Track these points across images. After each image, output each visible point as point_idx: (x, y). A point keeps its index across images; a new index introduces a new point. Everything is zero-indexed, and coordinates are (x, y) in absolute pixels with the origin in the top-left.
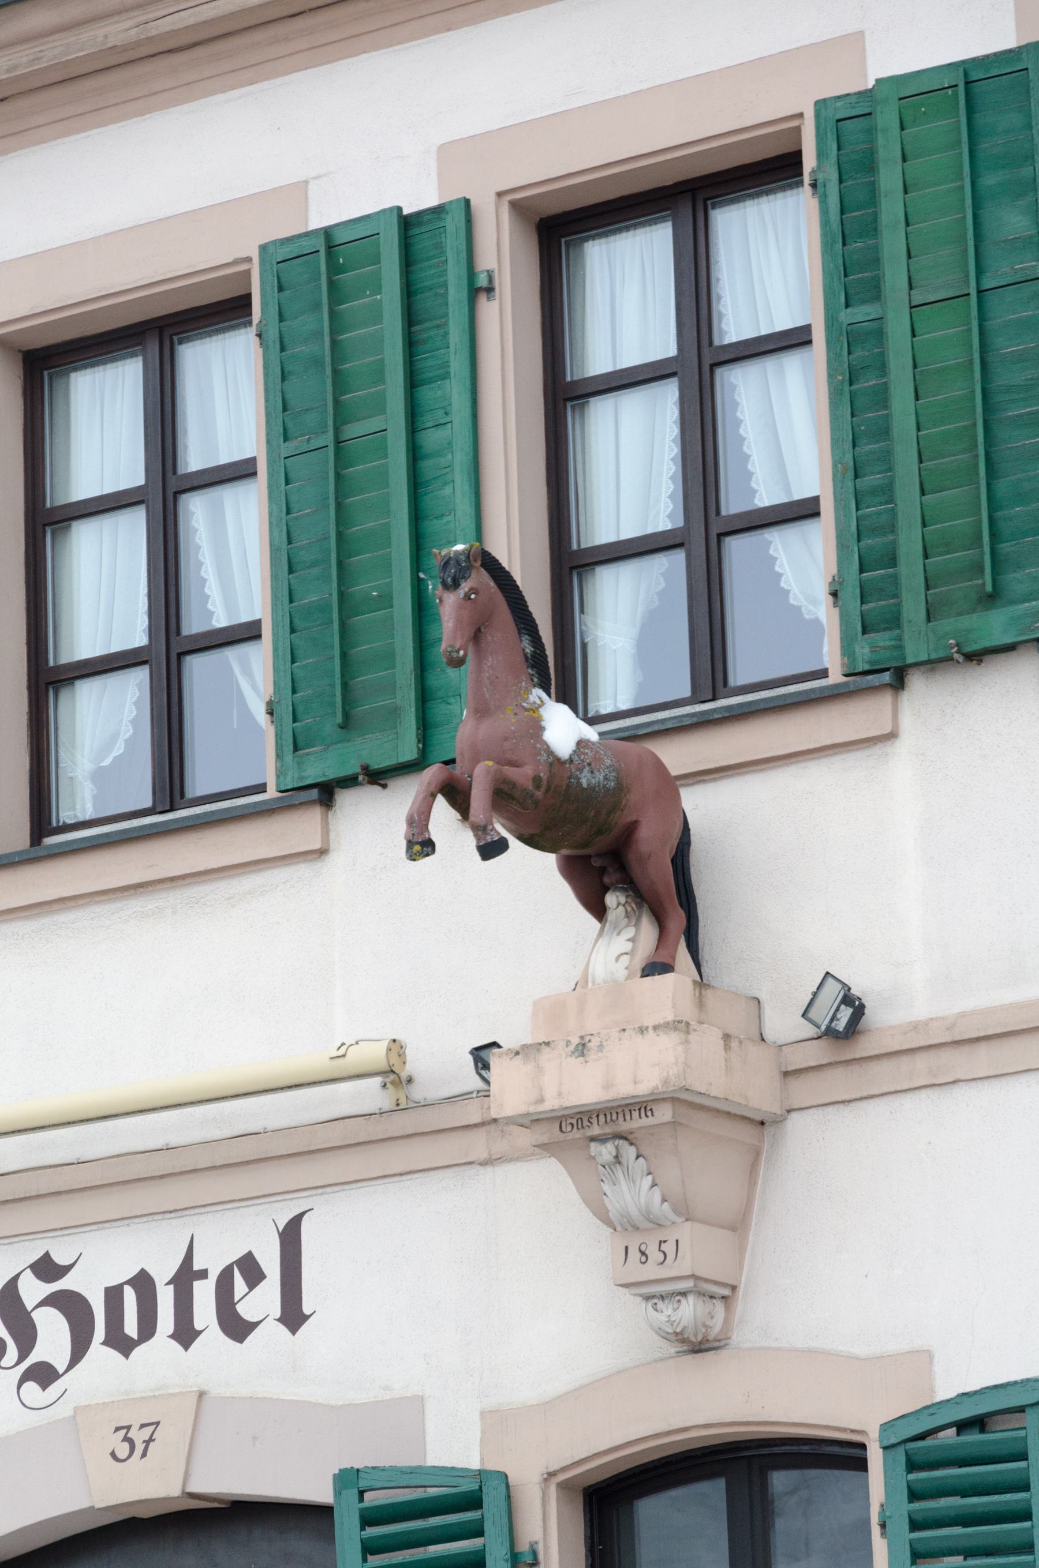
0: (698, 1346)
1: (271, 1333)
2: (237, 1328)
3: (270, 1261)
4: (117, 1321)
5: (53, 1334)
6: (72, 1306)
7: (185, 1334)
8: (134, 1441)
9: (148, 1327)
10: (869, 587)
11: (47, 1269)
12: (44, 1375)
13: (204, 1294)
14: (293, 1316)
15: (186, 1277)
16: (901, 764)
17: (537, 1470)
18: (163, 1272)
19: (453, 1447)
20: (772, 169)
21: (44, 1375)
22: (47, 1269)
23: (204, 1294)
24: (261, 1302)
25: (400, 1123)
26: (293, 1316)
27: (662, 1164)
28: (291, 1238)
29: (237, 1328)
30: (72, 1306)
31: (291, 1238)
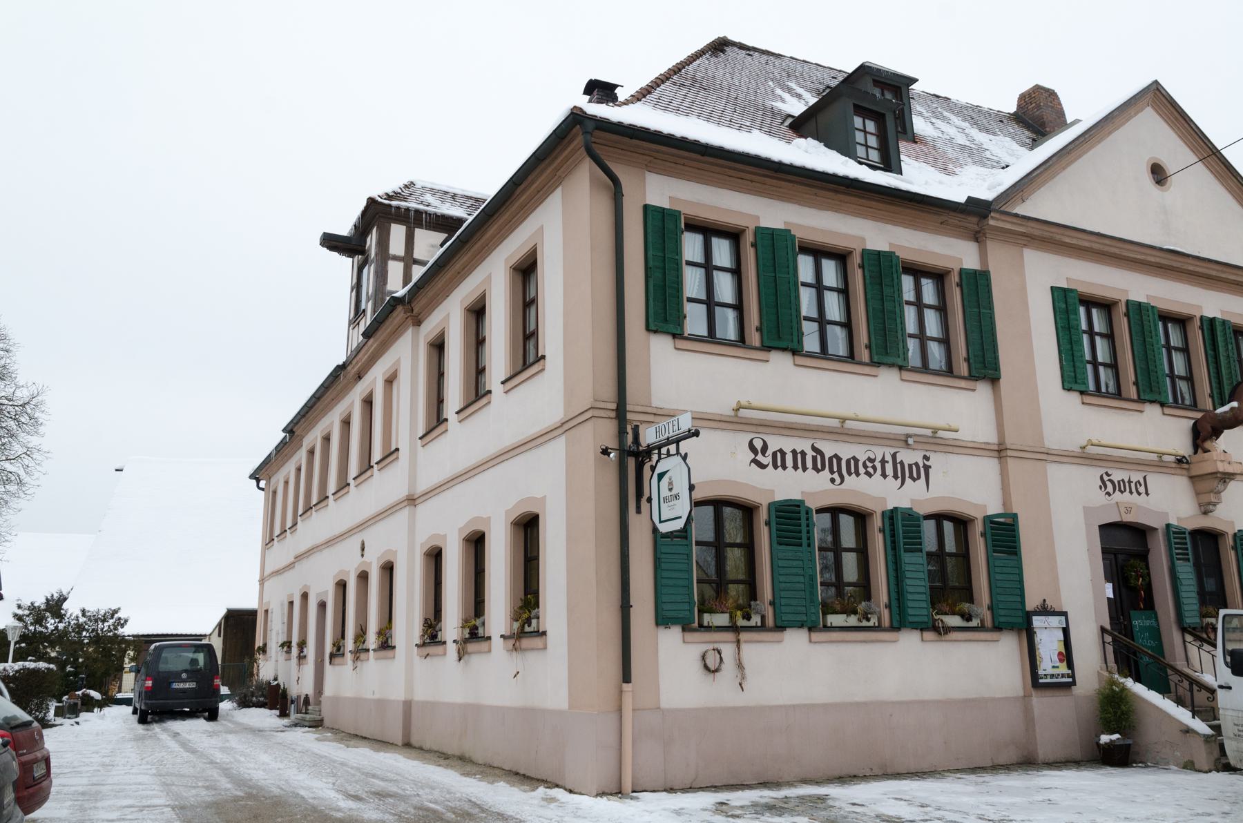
1: (1144, 495)
5: (1110, 488)
14: (1147, 494)
24: (1142, 489)
26: (1147, 494)
28: (1145, 478)
29: (1139, 494)
31: (1145, 478)
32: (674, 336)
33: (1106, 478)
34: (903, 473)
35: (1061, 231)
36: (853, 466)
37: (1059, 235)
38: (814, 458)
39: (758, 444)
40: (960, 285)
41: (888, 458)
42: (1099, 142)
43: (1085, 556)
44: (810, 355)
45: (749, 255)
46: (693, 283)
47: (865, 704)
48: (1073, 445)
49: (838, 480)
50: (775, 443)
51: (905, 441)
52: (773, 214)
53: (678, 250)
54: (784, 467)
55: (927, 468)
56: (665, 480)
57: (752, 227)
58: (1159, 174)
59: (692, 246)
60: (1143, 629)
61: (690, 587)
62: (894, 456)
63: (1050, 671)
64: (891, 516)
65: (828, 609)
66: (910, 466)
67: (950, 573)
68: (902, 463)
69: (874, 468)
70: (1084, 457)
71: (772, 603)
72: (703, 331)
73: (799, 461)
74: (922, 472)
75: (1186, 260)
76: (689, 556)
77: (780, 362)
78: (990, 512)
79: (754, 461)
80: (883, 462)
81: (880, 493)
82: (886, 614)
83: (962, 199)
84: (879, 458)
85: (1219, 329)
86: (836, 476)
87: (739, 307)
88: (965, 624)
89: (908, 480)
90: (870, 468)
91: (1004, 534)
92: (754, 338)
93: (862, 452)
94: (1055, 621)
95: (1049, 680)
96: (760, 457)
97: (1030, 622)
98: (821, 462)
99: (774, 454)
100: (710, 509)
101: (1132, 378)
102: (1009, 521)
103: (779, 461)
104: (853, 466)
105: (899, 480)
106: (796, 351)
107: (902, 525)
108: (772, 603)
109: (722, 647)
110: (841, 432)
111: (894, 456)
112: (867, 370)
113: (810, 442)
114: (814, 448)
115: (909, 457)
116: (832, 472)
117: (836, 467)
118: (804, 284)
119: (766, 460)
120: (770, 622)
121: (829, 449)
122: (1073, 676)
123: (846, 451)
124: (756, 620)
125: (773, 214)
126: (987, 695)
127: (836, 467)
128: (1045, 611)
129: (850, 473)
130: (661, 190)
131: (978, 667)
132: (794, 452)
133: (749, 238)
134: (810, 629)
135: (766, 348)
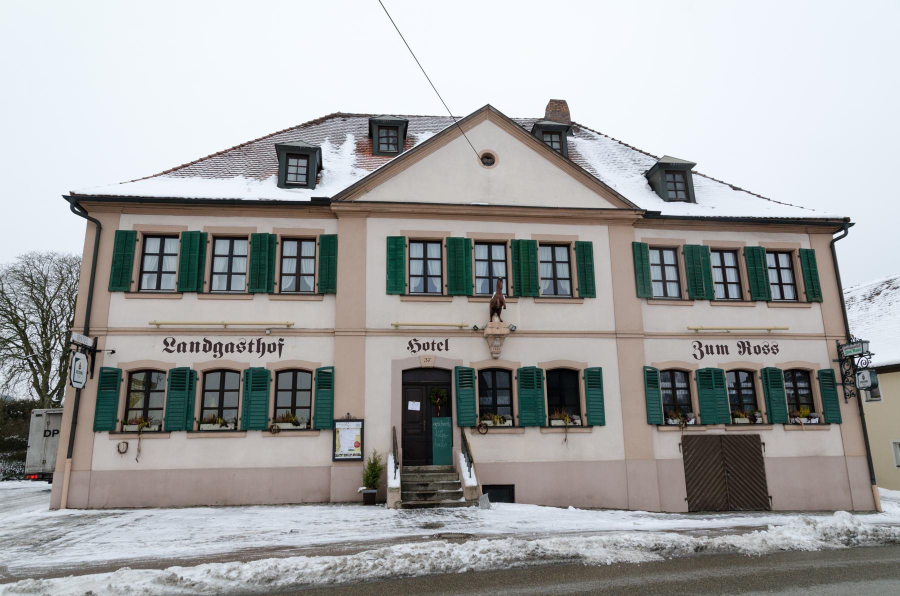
0: (496, 358)
1: (444, 351)
2: (440, 350)
3: (444, 343)
4: (426, 346)
5: (416, 348)
6: (419, 345)
7: (750, 353)
8: (427, 360)
9: (227, 346)
10: (179, 283)
11: (415, 340)
12: (415, 352)
13: (436, 346)
14: (447, 349)
15: (433, 344)
16: (518, 305)
17: (476, 368)
18: (430, 343)
19: (466, 365)
20: (175, 236)
21: (415, 352)
22: (415, 340)
23: (436, 346)
24: (443, 347)
25: (460, 331)
26: (447, 349)
27: (495, 340)
28: (446, 341)
29: (440, 350)
30: (419, 345)
31: (446, 341)
32: (767, 302)
33: (413, 342)
34: (262, 348)
35: (599, 212)
36: (230, 348)
37: (386, 208)
38: (205, 346)
39: (170, 341)
40: (800, 256)
41: (255, 342)
42: (438, 148)
43: (389, 388)
44: (658, 299)
45: (573, 254)
46: (655, 273)
47: (218, 469)
48: (387, 325)
49: (699, 356)
50: (179, 340)
51: (263, 332)
52: (752, 239)
53: (647, 259)
54: (712, 353)
55: (281, 346)
56: (78, 362)
57: (682, 245)
58: (488, 159)
59: (654, 257)
60: (439, 428)
61: (660, 408)
62: (259, 341)
63: (346, 451)
64: (765, 371)
65: (734, 416)
66: (269, 345)
67: (303, 400)
68: (264, 344)
69: (244, 348)
70: (397, 331)
71: (823, 413)
72: (779, 297)
73: (195, 347)
74: (775, 350)
75: (362, 205)
76: (659, 394)
77: (761, 306)
78: (822, 368)
79: (166, 349)
80: (251, 344)
81: (759, 362)
82: (765, 417)
83: (310, 200)
84: (248, 342)
85: (521, 246)
86: (218, 354)
87: (678, 282)
88: (295, 427)
89: (266, 352)
90: (241, 348)
91: (325, 379)
92: (747, 296)
93: (236, 341)
94: (356, 426)
95: (343, 457)
96: (170, 347)
97: (334, 425)
98: (208, 346)
99: (179, 346)
100: (733, 373)
101: (803, 290)
102: (330, 371)
103: (182, 348)
104: (230, 348)
105: (260, 353)
106: (768, 300)
107: (772, 376)
108: (823, 413)
109: (130, 442)
110: (225, 330)
111: (259, 341)
112: (750, 304)
113: (203, 338)
114: (205, 340)
115: (267, 340)
116: (215, 351)
117: (218, 349)
118: (770, 268)
119: (175, 348)
120: (585, 423)
121: (214, 340)
122: (362, 455)
123: (225, 340)
124: (692, 422)
125: (752, 239)
126: (304, 465)
127: (218, 349)
128: (348, 419)
129: (708, 353)
130: (128, 222)
131: (306, 451)
132: (717, 346)
133: (681, 250)
134: (784, 424)
135: (754, 300)
